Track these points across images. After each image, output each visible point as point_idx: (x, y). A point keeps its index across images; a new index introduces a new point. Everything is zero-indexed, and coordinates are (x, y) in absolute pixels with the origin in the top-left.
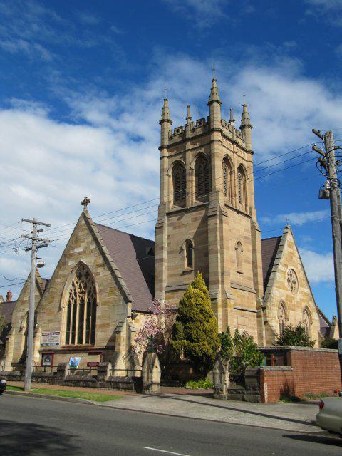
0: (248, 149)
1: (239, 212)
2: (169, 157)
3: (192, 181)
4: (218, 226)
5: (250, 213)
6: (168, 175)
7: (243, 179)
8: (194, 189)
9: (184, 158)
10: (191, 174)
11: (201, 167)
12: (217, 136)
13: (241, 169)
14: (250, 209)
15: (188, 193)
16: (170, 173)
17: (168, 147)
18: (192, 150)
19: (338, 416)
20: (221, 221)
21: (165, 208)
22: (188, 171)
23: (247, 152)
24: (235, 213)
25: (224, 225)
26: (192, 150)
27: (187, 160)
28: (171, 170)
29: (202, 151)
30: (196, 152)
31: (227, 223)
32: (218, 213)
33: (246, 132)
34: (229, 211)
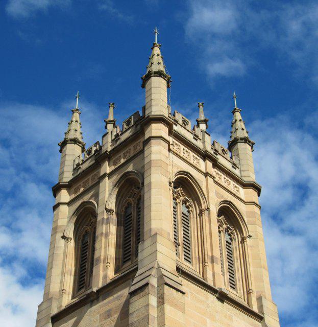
0: (246, 179)
1: (223, 297)
2: (69, 204)
3: (107, 235)
4: (153, 312)
5: (261, 307)
6: (64, 237)
7: (237, 238)
8: (112, 251)
9: (96, 196)
10: (108, 221)
11: (129, 204)
12: (158, 129)
13: (228, 213)
14: (259, 299)
15: (98, 260)
16: (70, 234)
17: (69, 186)
18: (110, 175)
19: (125, 141)
20: (161, 300)
21: (50, 307)
22: (102, 215)
23: (245, 185)
24: (212, 298)
25: (167, 307)
26: (110, 175)
27: (100, 197)
28: (72, 228)
29: (130, 168)
30: (116, 178)
31: (181, 308)
32: (154, 281)
33: (240, 151)
34: (187, 285)
